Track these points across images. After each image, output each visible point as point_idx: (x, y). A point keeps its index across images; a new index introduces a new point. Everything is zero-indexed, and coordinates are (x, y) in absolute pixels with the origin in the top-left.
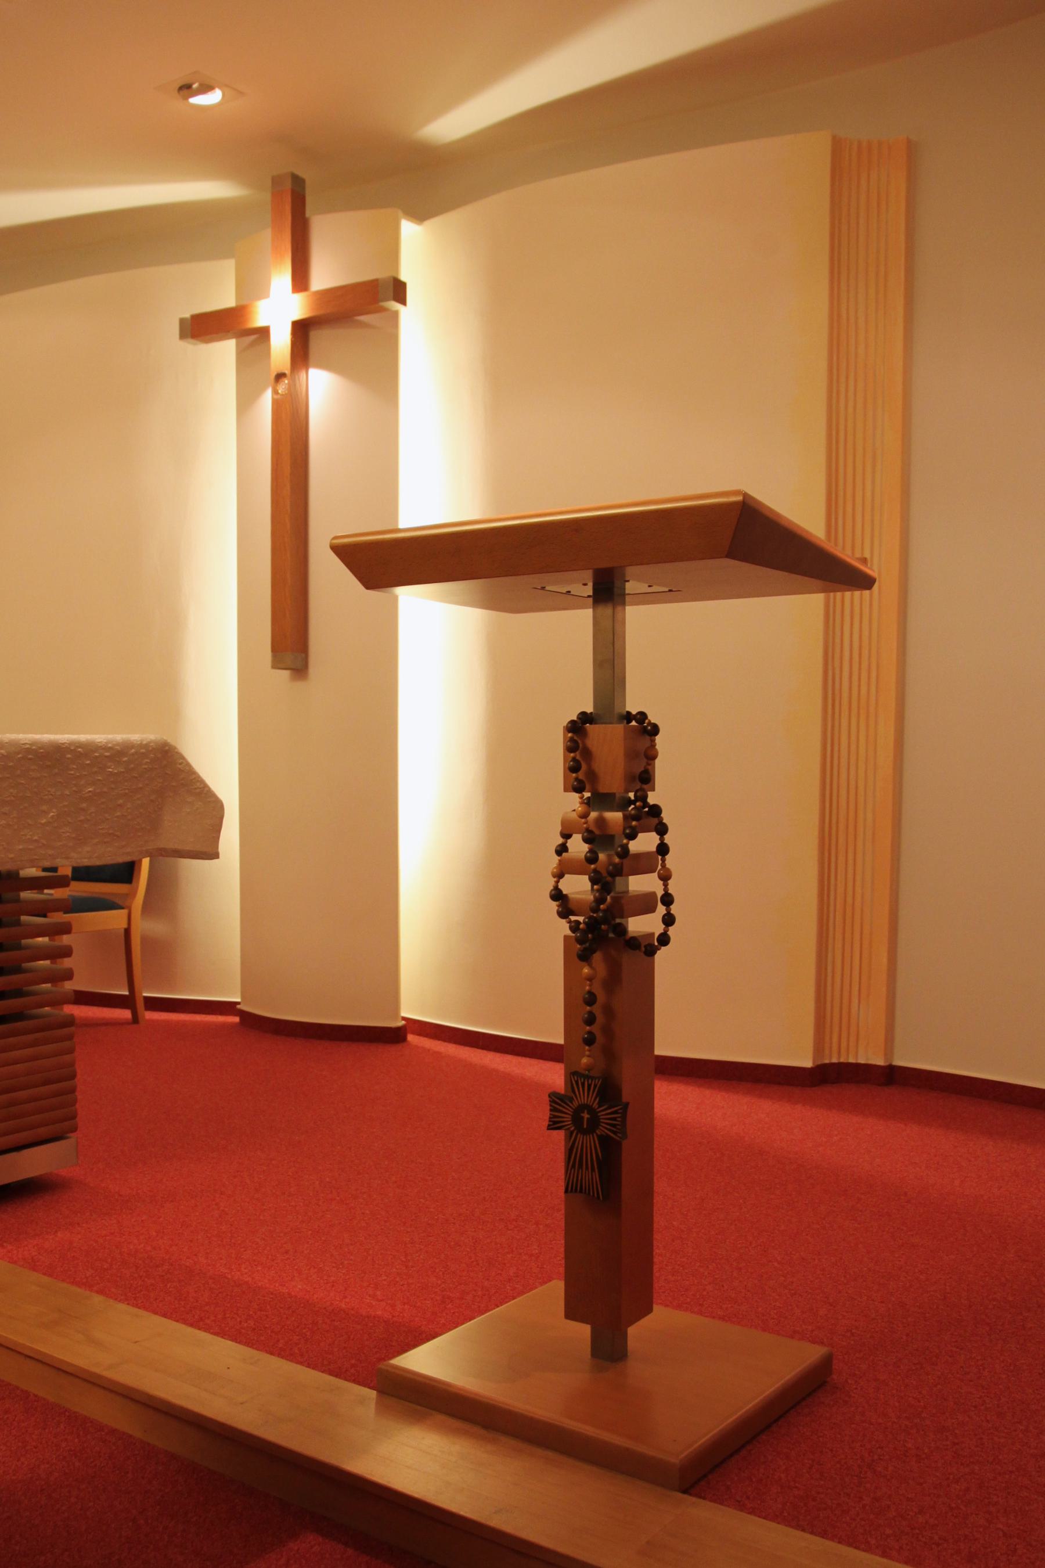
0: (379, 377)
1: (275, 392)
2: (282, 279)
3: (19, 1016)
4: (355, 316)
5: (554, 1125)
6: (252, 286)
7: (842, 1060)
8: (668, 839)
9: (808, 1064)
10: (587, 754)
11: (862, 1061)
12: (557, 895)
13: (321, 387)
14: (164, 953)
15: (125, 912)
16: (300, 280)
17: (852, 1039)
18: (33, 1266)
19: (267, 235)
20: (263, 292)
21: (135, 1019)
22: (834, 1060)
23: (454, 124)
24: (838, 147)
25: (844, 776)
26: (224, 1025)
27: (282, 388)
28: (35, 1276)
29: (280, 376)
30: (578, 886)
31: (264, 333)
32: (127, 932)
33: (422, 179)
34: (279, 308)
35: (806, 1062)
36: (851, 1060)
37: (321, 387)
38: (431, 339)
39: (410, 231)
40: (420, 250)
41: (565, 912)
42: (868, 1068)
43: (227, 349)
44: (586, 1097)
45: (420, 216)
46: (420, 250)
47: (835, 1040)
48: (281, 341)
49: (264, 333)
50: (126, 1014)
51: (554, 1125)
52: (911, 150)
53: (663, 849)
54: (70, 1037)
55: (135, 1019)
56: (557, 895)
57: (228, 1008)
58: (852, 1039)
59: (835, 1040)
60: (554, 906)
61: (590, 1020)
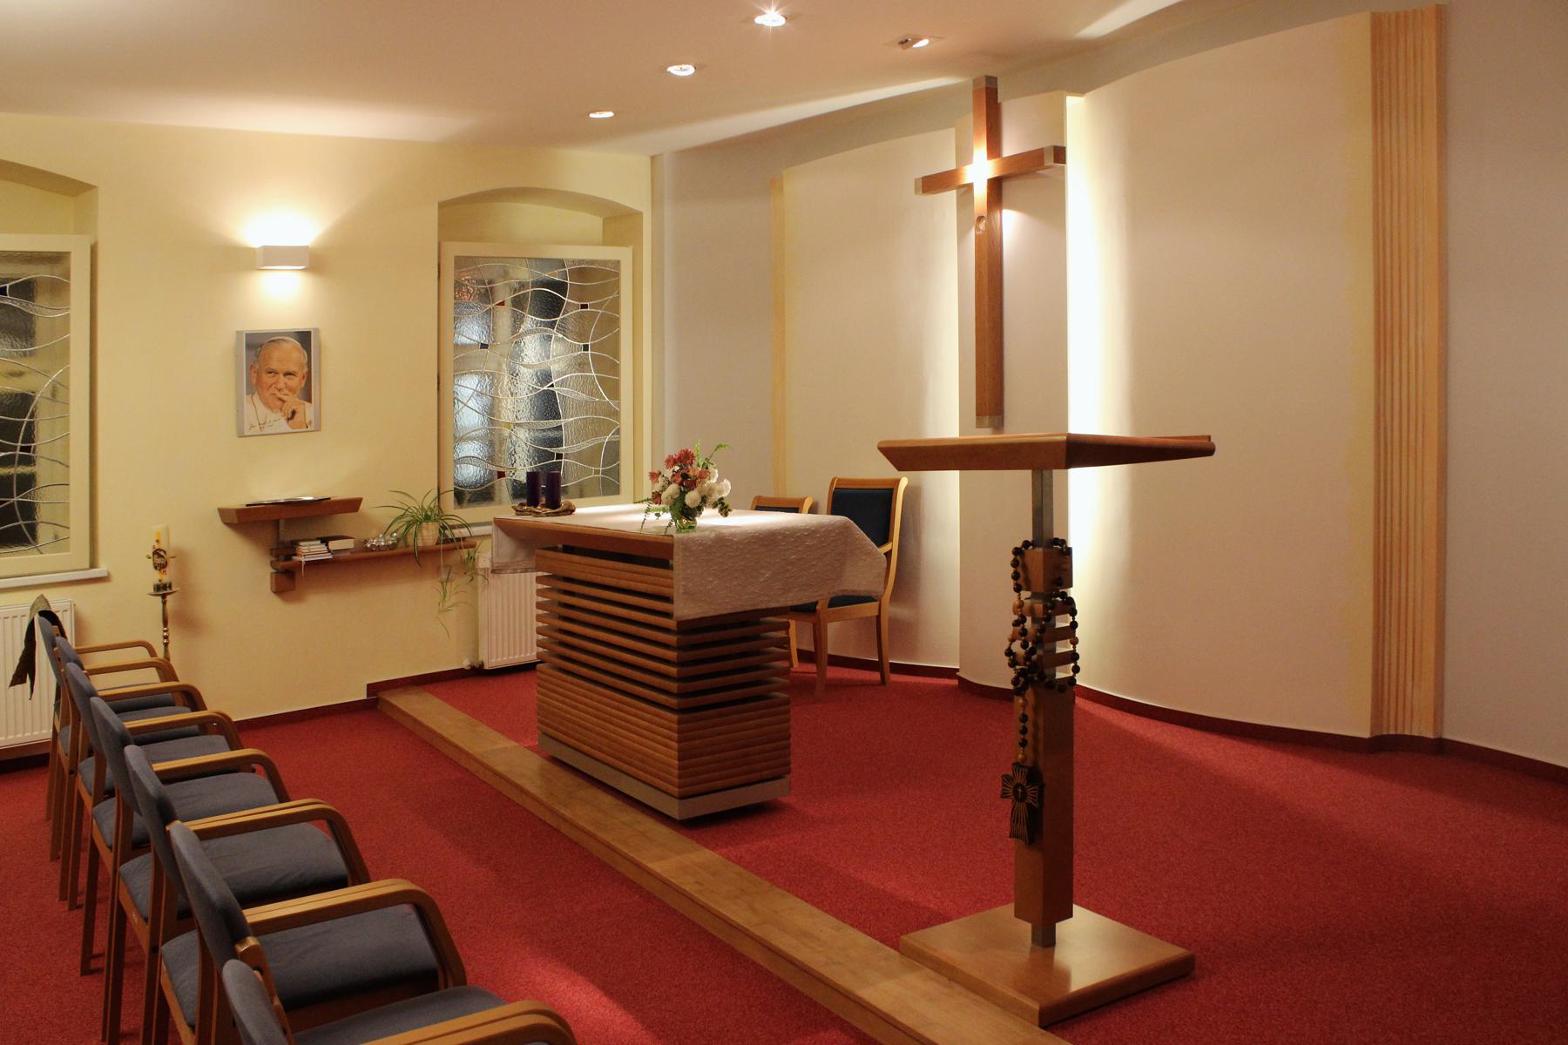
0: (1052, 212)
1: (977, 229)
2: (980, 150)
3: (760, 698)
4: (1033, 173)
5: (1004, 795)
6: (964, 156)
7: (1399, 732)
8: (1077, 618)
9: (1366, 734)
10: (1025, 567)
11: (1415, 733)
12: (1009, 652)
13: (1011, 222)
14: (906, 631)
15: (876, 604)
16: (994, 148)
17: (1408, 715)
18: (739, 861)
19: (970, 117)
20: (969, 161)
21: (883, 681)
22: (1392, 732)
23: (1100, 27)
24: (1377, 22)
25: (1396, 504)
26: (946, 686)
27: (982, 226)
28: (737, 868)
29: (980, 218)
30: (1017, 647)
31: (970, 187)
32: (878, 617)
33: (1080, 65)
34: (980, 170)
35: (1365, 733)
36: (1407, 733)
37: (1011, 222)
38: (1088, 184)
39: (1075, 106)
40: (1082, 120)
41: (1013, 664)
42: (1421, 739)
43: (951, 196)
44: (1020, 779)
45: (1080, 91)
46: (1082, 120)
47: (1392, 713)
48: (981, 193)
49: (970, 187)
50: (876, 676)
51: (1004, 795)
52: (1441, 14)
53: (1074, 625)
54: (788, 712)
55: (883, 681)
56: (1009, 652)
57: (951, 673)
58: (1408, 715)
59: (1392, 713)
60: (1006, 659)
61: (1024, 731)
